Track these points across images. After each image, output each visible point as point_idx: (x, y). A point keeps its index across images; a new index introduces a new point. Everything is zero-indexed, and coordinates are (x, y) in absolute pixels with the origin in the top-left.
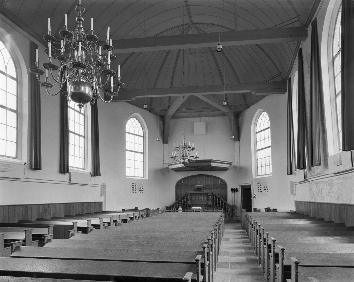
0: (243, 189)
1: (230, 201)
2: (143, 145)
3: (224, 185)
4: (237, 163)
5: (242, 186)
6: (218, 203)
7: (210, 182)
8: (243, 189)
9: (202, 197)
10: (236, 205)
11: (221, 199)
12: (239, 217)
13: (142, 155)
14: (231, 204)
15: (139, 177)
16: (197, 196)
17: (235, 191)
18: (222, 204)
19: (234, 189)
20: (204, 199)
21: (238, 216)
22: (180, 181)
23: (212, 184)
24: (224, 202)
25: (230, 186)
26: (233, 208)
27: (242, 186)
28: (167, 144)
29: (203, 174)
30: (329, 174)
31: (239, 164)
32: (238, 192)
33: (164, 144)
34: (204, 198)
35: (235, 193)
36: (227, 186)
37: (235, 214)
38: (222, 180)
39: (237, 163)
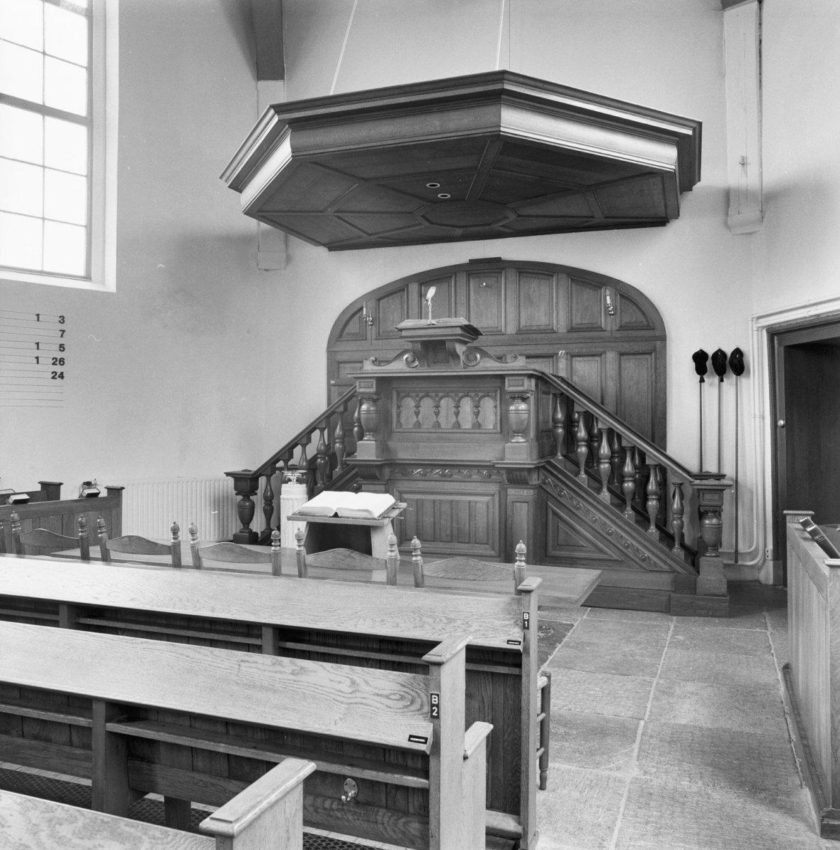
0: (791, 350)
1: (682, 444)
2: (90, 69)
3: (641, 328)
4: (743, 164)
5: (775, 334)
6: (561, 439)
7: (550, 310)
8: (791, 350)
9: (467, 405)
10: (728, 470)
11: (604, 422)
12: (753, 555)
13: (82, 131)
14: (693, 466)
15: (41, 273)
16: (427, 404)
17: (721, 372)
18: (642, 483)
19: (719, 355)
20: (477, 425)
21: (742, 548)
22: (352, 314)
23: (561, 324)
24: (633, 449)
25: (686, 337)
26: (717, 514)
27: (775, 334)
28: (279, 83)
29: (498, 260)
30: (440, 656)
31: (753, 169)
32: (743, 380)
33: (262, 84)
34: (477, 414)
35: (724, 384)
36: (663, 338)
37: (717, 544)
38: (628, 296)
39: (743, 164)
